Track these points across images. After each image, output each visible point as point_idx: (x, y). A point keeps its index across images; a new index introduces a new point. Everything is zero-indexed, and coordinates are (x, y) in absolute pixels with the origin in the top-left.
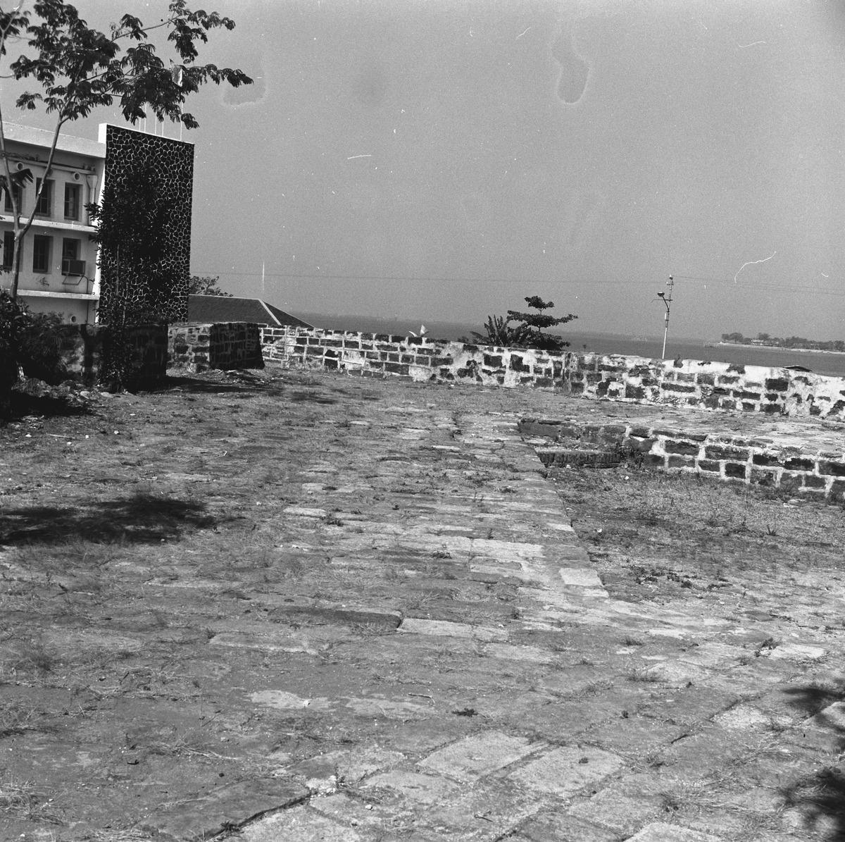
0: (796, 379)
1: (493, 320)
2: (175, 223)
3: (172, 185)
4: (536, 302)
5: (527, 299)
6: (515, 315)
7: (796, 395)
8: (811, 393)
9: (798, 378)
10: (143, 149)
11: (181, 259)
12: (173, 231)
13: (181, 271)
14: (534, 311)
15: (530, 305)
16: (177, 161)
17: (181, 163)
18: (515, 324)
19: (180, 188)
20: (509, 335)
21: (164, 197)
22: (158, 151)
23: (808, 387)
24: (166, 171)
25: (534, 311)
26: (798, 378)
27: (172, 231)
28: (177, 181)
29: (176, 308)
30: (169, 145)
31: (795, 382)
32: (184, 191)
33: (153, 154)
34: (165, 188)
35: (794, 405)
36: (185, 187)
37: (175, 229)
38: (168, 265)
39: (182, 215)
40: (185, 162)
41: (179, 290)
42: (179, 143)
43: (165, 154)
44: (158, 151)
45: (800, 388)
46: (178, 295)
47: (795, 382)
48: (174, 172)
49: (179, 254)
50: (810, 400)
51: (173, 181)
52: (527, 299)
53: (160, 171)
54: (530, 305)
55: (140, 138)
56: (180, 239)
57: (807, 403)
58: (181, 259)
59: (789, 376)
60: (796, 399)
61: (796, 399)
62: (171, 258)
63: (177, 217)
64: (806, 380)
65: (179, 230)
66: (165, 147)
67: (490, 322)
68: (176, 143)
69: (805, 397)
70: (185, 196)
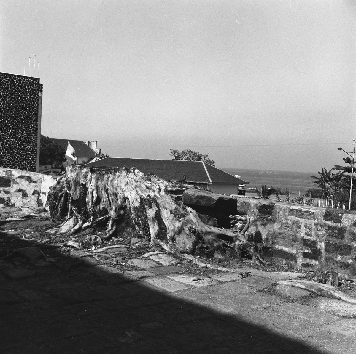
0: (19, 177)
1: (324, 170)
2: (27, 116)
3: (24, 98)
4: (348, 161)
5: (344, 159)
6: (338, 167)
7: (20, 190)
8: (36, 189)
9: (21, 177)
10: (4, 81)
11: (31, 134)
12: (25, 120)
13: (32, 140)
14: (348, 165)
15: (346, 162)
16: (28, 86)
17: (31, 87)
18: (335, 172)
19: (30, 100)
20: (331, 177)
21: (19, 103)
22: (15, 82)
23: (32, 184)
24: (20, 91)
25: (348, 165)
26: (21, 177)
27: (25, 120)
28: (28, 96)
29: (28, 158)
30: (22, 78)
31: (18, 180)
32: (33, 101)
33: (11, 83)
34: (19, 99)
35: (19, 198)
36: (34, 99)
37: (27, 119)
38: (23, 137)
39: (31, 112)
40: (33, 87)
41: (30, 149)
42: (29, 78)
43: (20, 83)
44: (15, 82)
45: (24, 185)
46: (30, 151)
47: (18, 180)
48: (26, 92)
49: (30, 131)
50: (37, 195)
51: (25, 96)
52: (344, 159)
53: (16, 91)
54: (346, 162)
55: (2, 75)
56: (30, 124)
57: (33, 197)
58: (31, 134)
59: (11, 175)
60: (21, 194)
61: (21, 194)
62: (25, 133)
63: (28, 113)
64: (29, 179)
65: (30, 120)
66: (19, 80)
67: (323, 171)
68: (27, 77)
69: (30, 191)
70: (34, 103)
